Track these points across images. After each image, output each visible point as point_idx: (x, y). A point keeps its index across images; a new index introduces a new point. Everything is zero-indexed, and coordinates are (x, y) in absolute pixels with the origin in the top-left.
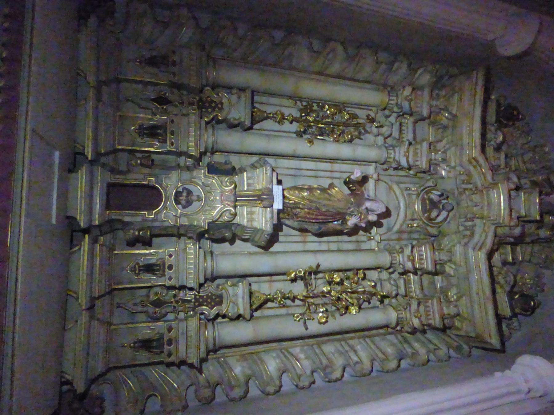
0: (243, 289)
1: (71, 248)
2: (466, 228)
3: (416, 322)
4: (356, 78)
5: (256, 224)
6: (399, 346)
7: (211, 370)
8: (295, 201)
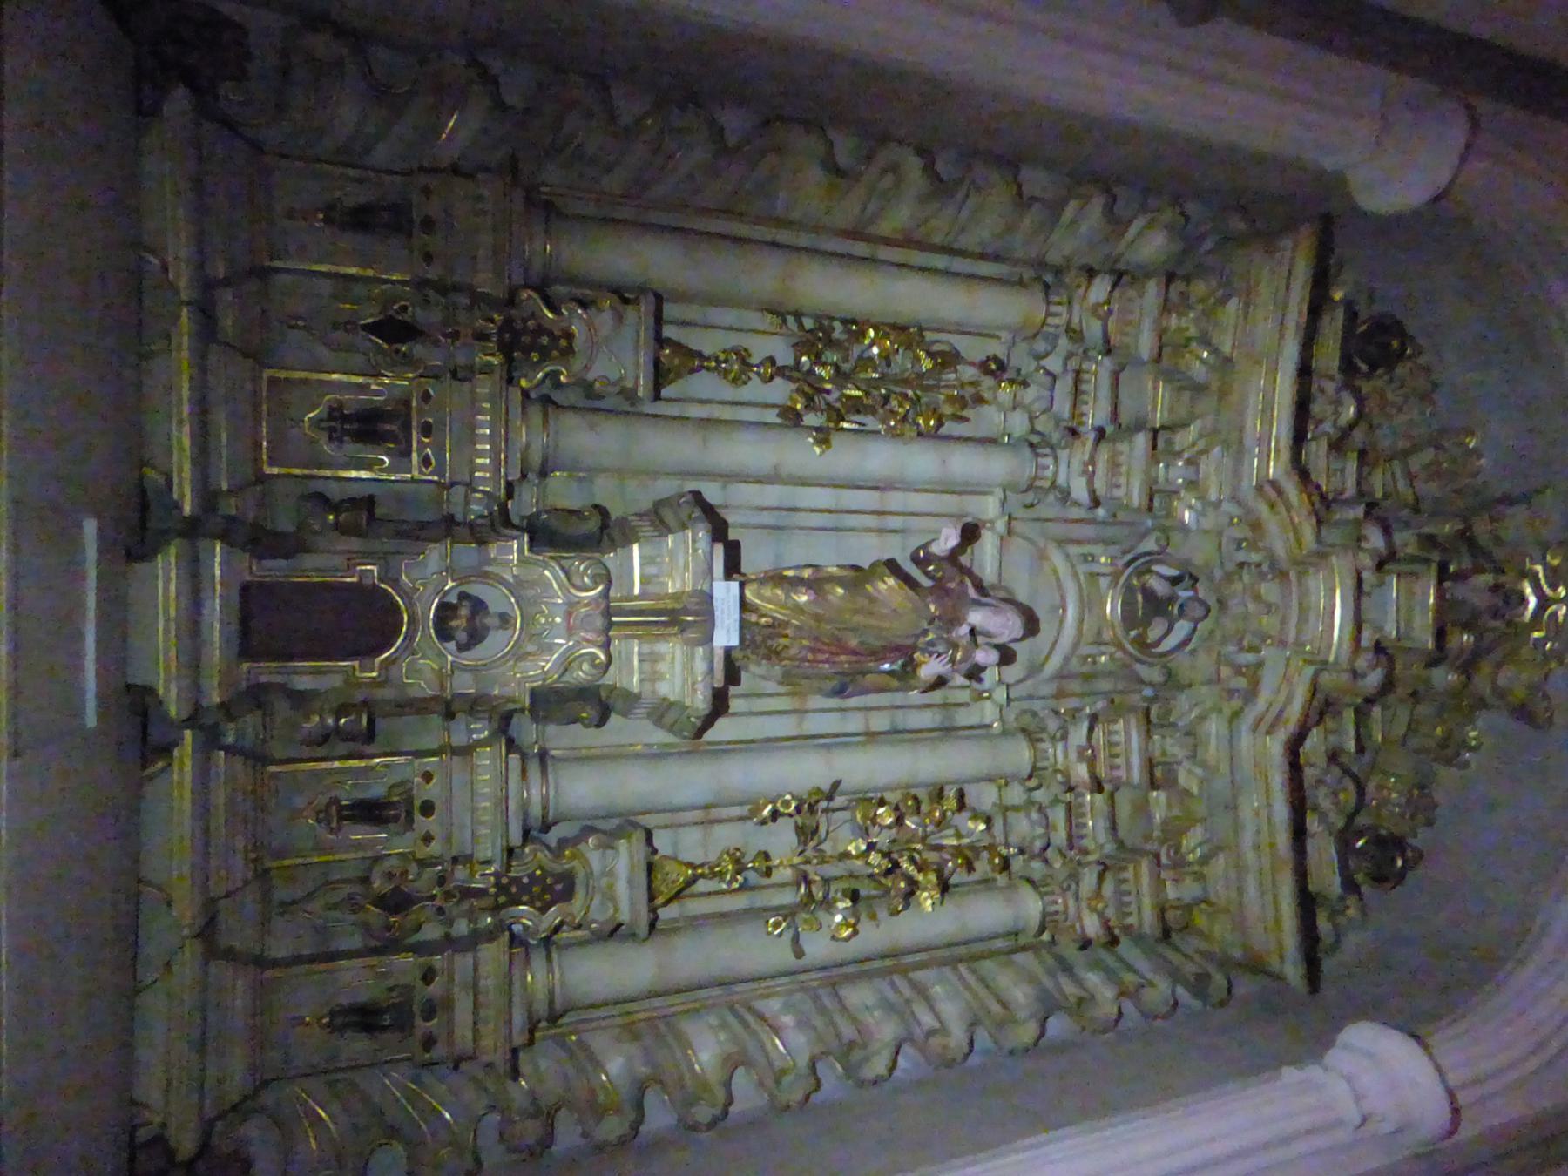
0: (631, 857)
1: (144, 767)
2: (1238, 670)
3: (1091, 926)
4: (956, 246)
5: (664, 689)
6: (1048, 982)
7: (545, 1069)
8: (774, 618)
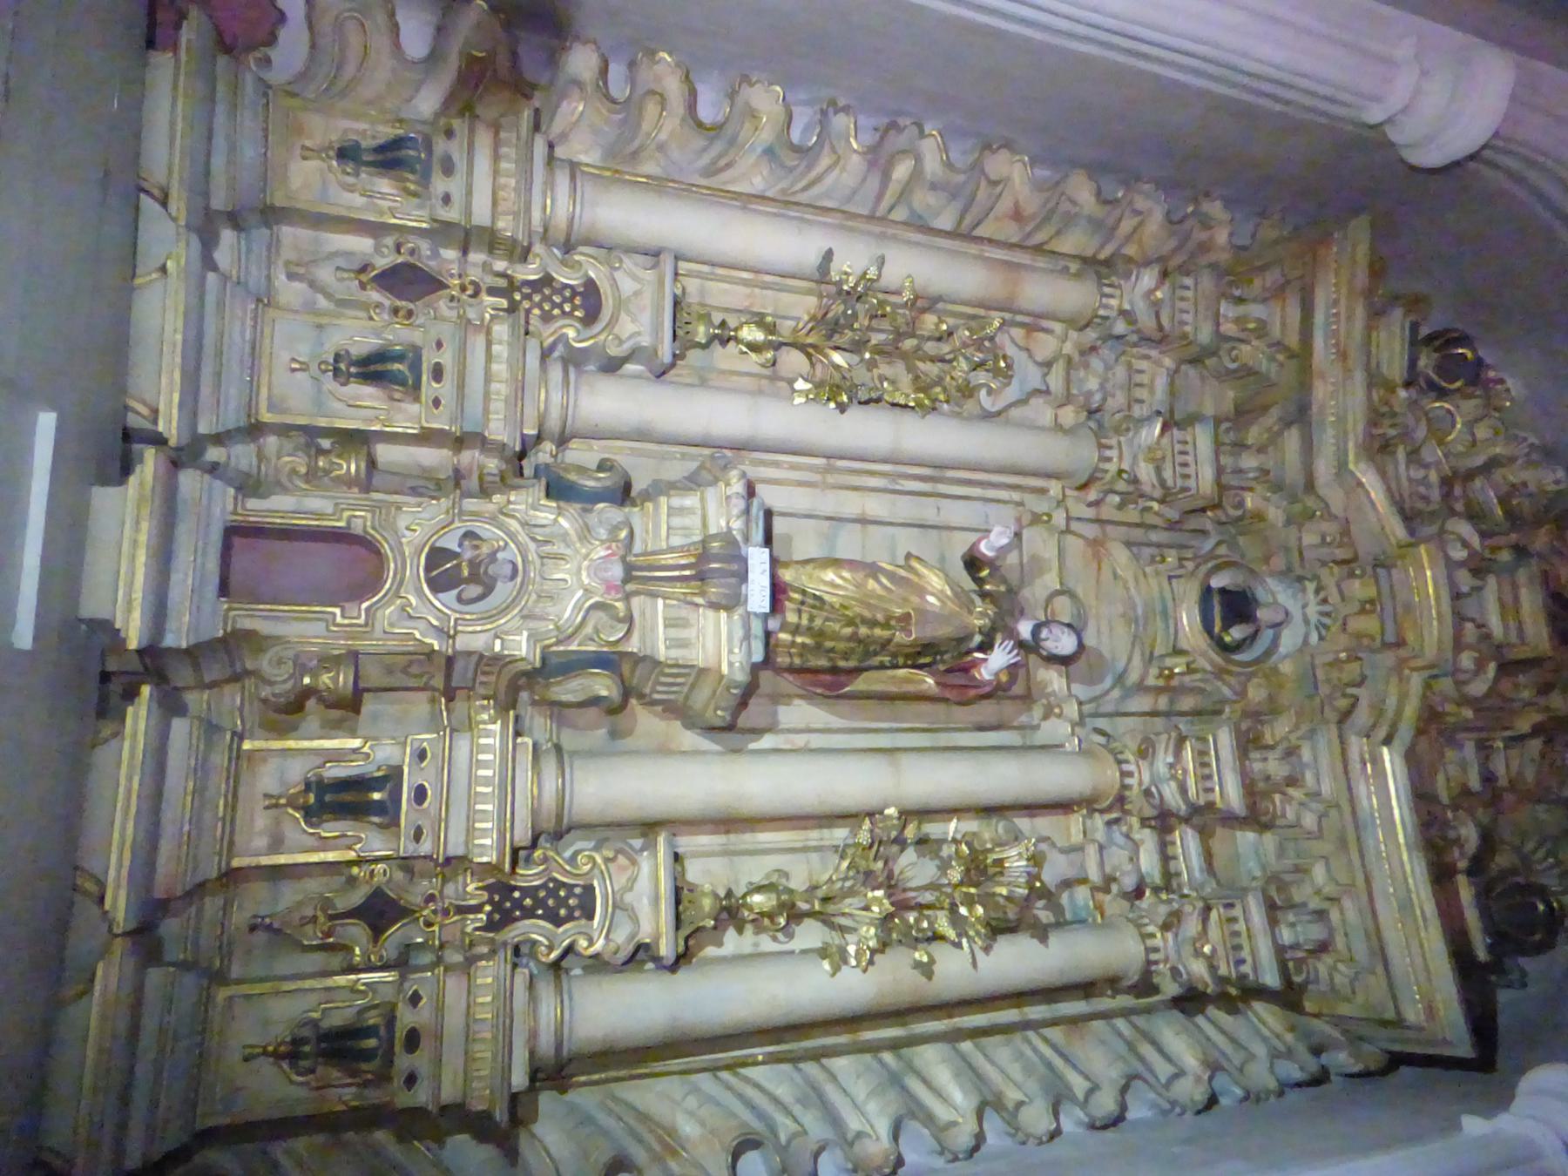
5: (699, 656)
